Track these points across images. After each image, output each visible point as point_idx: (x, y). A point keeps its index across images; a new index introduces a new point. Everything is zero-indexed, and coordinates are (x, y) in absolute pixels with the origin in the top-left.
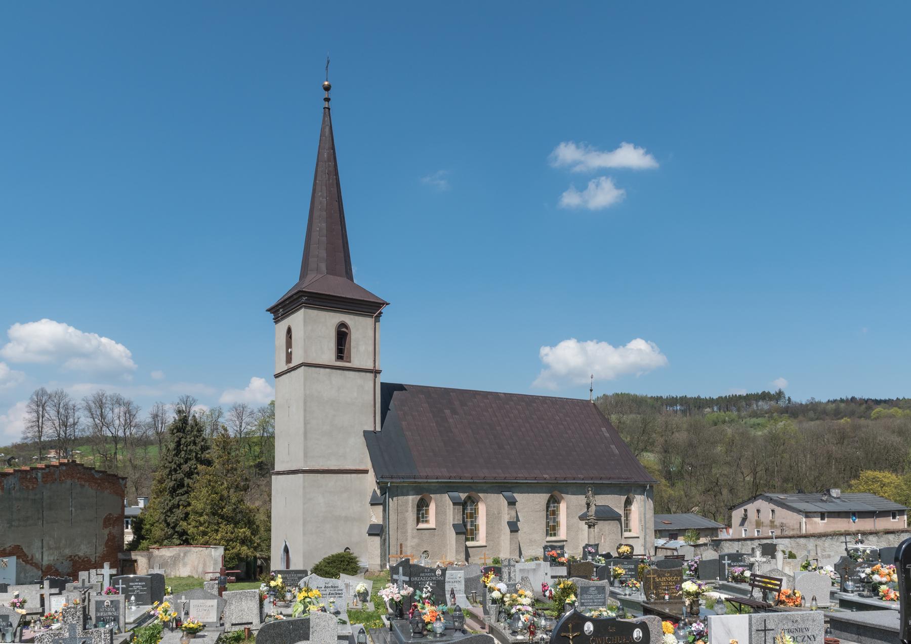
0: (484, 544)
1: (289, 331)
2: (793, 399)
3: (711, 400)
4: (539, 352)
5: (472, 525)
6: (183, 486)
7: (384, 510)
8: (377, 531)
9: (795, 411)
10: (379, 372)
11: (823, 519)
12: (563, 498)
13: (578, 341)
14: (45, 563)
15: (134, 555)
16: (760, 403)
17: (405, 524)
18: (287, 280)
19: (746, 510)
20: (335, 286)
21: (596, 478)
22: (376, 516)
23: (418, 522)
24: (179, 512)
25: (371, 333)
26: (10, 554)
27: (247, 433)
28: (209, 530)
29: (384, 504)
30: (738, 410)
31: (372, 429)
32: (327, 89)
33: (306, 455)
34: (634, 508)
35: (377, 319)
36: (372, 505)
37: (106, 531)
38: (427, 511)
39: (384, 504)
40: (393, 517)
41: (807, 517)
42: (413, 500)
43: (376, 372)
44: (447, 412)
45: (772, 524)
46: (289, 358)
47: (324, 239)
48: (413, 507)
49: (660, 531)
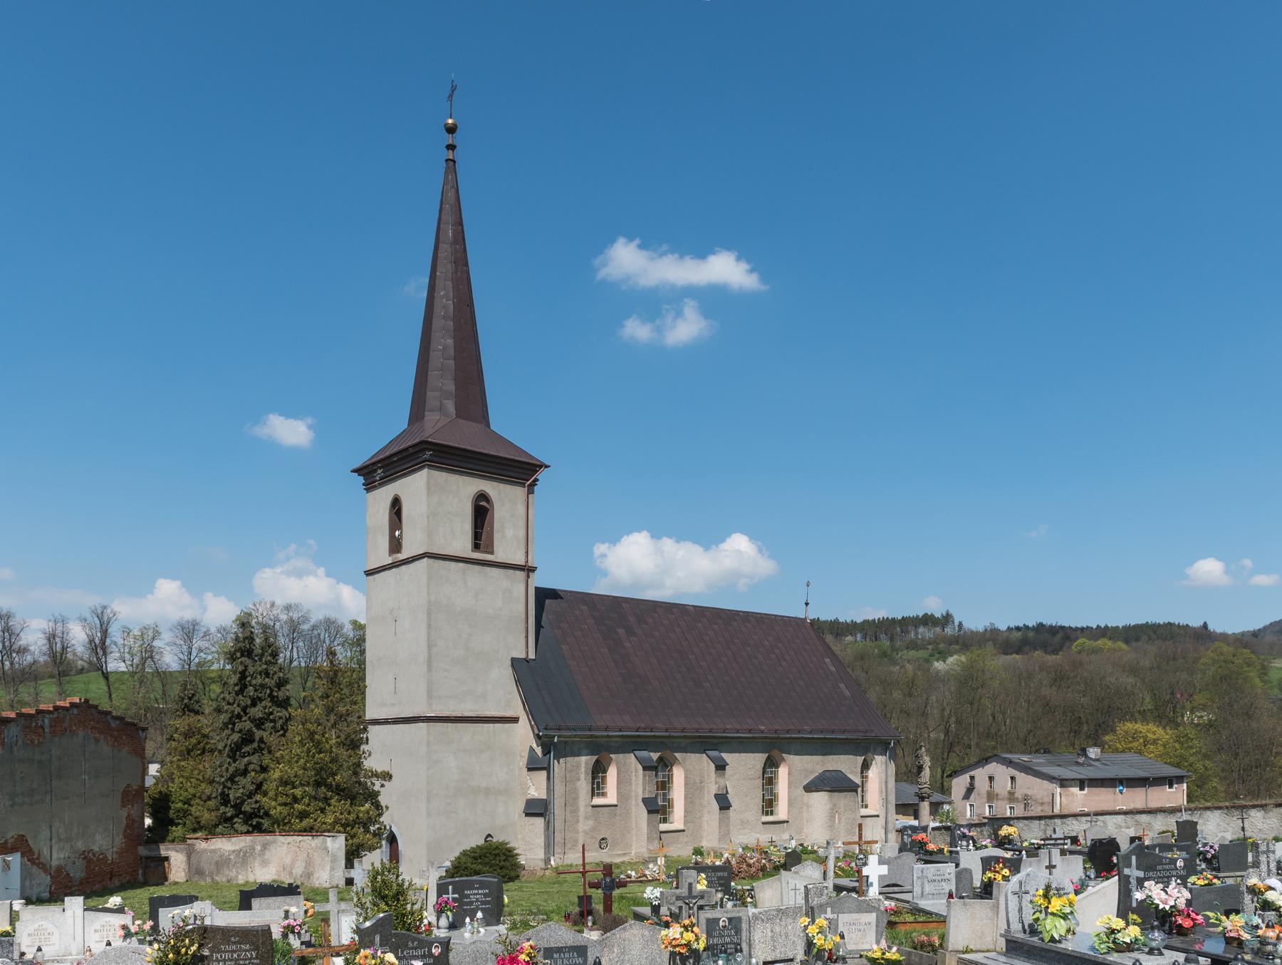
0: (682, 827)
1: (396, 505)
2: (966, 625)
3: (854, 624)
4: (591, 553)
5: (664, 800)
6: (252, 741)
7: (548, 778)
8: (537, 809)
9: (965, 641)
10: (532, 569)
11: (1082, 789)
12: (783, 759)
13: (652, 537)
14: (55, 863)
15: (164, 850)
16: (921, 630)
17: (576, 799)
18: (388, 425)
19: (972, 778)
20: (464, 437)
21: (827, 731)
22: (536, 787)
23: (593, 795)
24: (246, 783)
25: (521, 510)
26: (12, 850)
27: (199, 665)
28: (311, 809)
29: (547, 769)
30: (892, 639)
31: (523, 656)
32: (451, 130)
33: (430, 695)
34: (873, 773)
35: (531, 490)
36: (530, 769)
37: (124, 813)
38: (604, 778)
39: (547, 769)
40: (559, 787)
41: (1062, 786)
42: (586, 763)
43: (529, 570)
44: (621, 631)
45: (1011, 797)
46: (395, 545)
47: (452, 362)
48: (586, 773)
49: (904, 805)
